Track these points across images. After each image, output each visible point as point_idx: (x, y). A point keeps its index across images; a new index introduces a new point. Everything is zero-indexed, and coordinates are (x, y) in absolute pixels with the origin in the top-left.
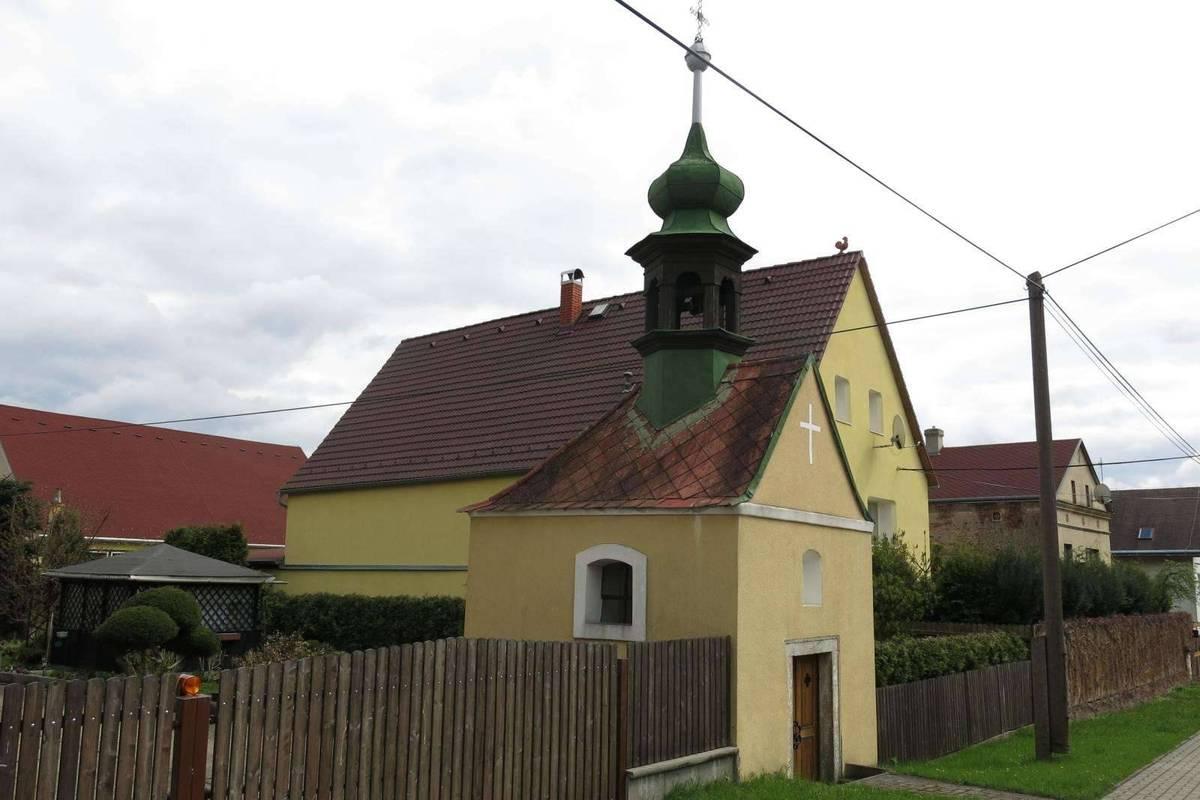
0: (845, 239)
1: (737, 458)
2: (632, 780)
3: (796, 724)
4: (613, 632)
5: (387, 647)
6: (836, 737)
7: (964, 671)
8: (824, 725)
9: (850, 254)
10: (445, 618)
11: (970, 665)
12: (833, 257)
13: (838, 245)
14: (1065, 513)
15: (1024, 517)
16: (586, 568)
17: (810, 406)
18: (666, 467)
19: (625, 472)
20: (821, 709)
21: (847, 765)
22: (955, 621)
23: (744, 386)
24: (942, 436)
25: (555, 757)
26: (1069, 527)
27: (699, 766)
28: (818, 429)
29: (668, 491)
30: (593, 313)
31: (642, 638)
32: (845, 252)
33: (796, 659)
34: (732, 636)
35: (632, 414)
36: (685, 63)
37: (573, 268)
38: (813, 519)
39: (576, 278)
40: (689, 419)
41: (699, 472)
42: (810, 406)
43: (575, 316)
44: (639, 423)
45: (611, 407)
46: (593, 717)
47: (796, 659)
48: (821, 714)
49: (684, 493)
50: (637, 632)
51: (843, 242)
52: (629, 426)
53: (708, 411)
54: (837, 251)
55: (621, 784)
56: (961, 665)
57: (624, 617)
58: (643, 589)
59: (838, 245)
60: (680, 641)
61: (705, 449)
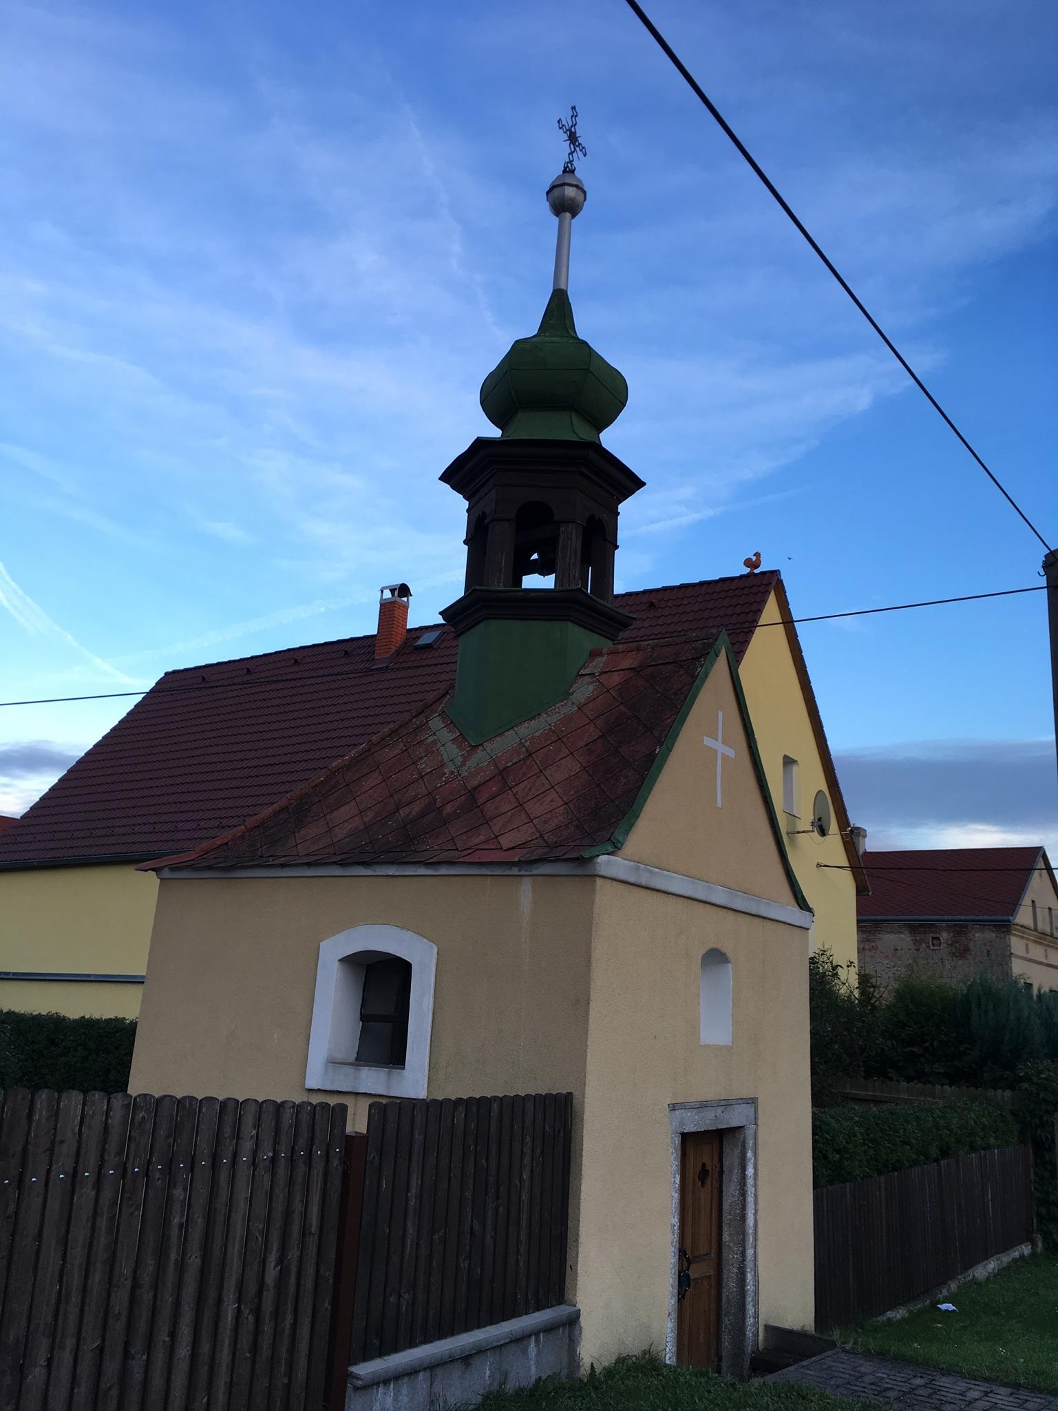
0: (757, 555)
1: (598, 785)
2: (356, 1389)
3: (682, 1253)
4: (373, 1081)
5: (109, 1093)
6: (749, 1276)
7: (937, 1160)
8: (731, 1256)
9: (763, 573)
10: (109, 1045)
11: (945, 1152)
12: (742, 577)
13: (748, 563)
14: (1025, 941)
15: (972, 944)
16: (336, 964)
17: (720, 713)
18: (480, 801)
19: (416, 808)
20: (725, 1228)
21: (767, 1328)
22: (909, 1079)
23: (616, 679)
24: (865, 836)
25: (183, 1352)
26: (1030, 960)
27: (504, 1349)
28: (731, 753)
29: (482, 838)
30: (420, 642)
31: (421, 1093)
32: (756, 571)
33: (685, 1137)
34: (576, 1094)
35: (436, 723)
36: (547, 205)
37: (397, 581)
38: (719, 897)
39: (400, 596)
40: (525, 730)
41: (535, 809)
42: (720, 713)
43: (398, 640)
44: (446, 736)
45: (407, 716)
46: (281, 1260)
47: (685, 1137)
48: (726, 1237)
49: (506, 841)
50: (413, 1081)
51: (754, 558)
52: (430, 739)
53: (555, 718)
54: (746, 570)
55: (334, 1387)
56: (934, 1151)
57: (395, 1057)
58: (428, 1002)
59: (748, 563)
60: (224, 1104)
61: (547, 773)
